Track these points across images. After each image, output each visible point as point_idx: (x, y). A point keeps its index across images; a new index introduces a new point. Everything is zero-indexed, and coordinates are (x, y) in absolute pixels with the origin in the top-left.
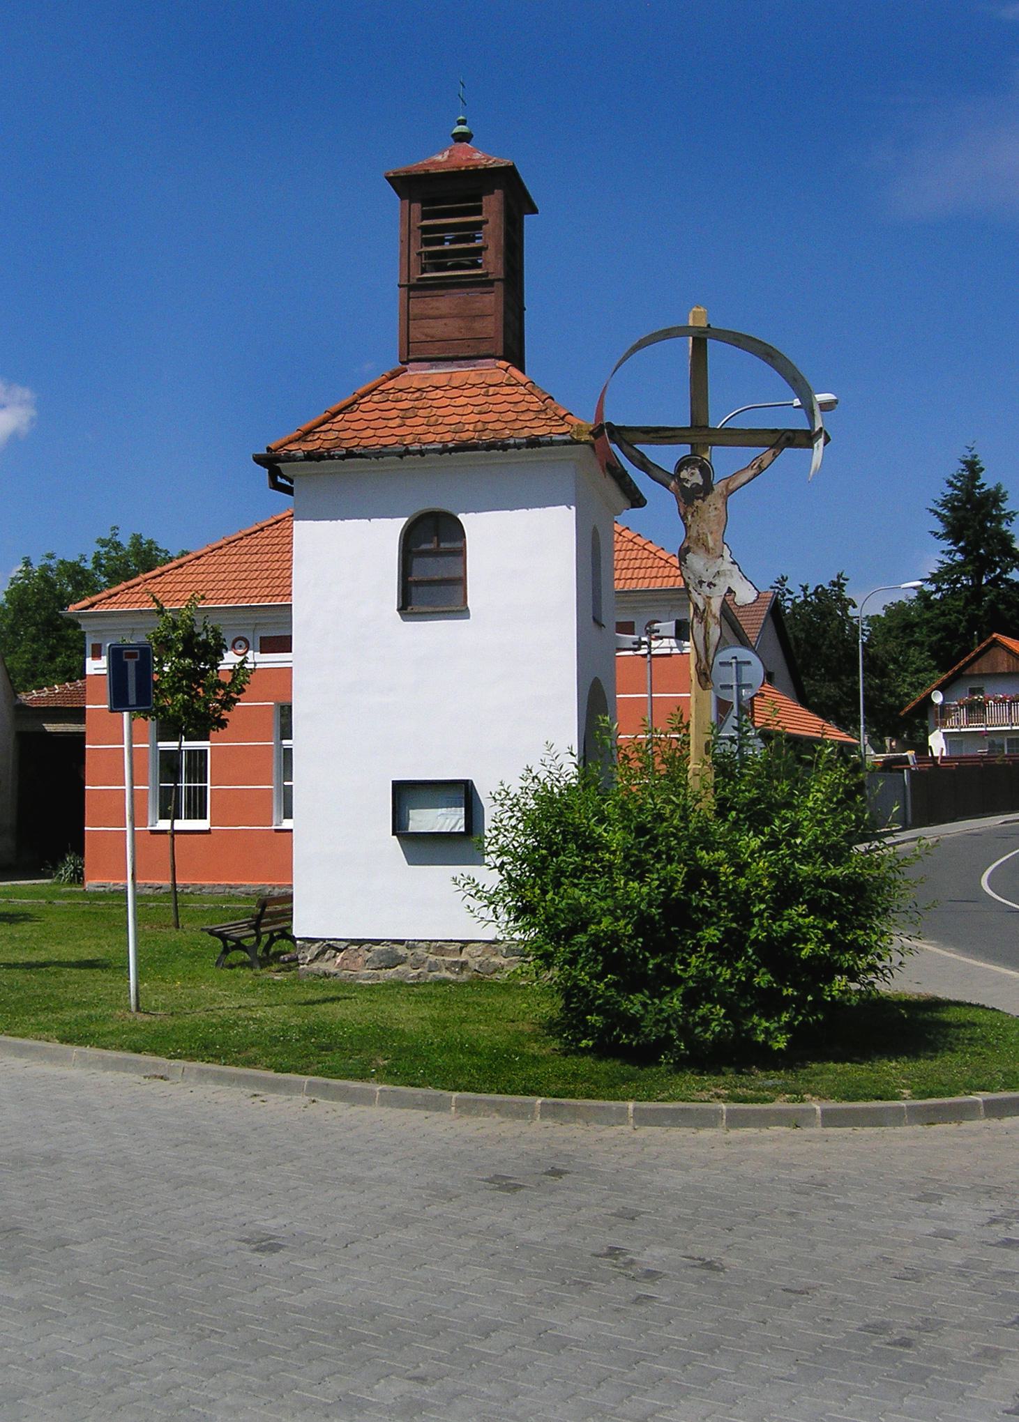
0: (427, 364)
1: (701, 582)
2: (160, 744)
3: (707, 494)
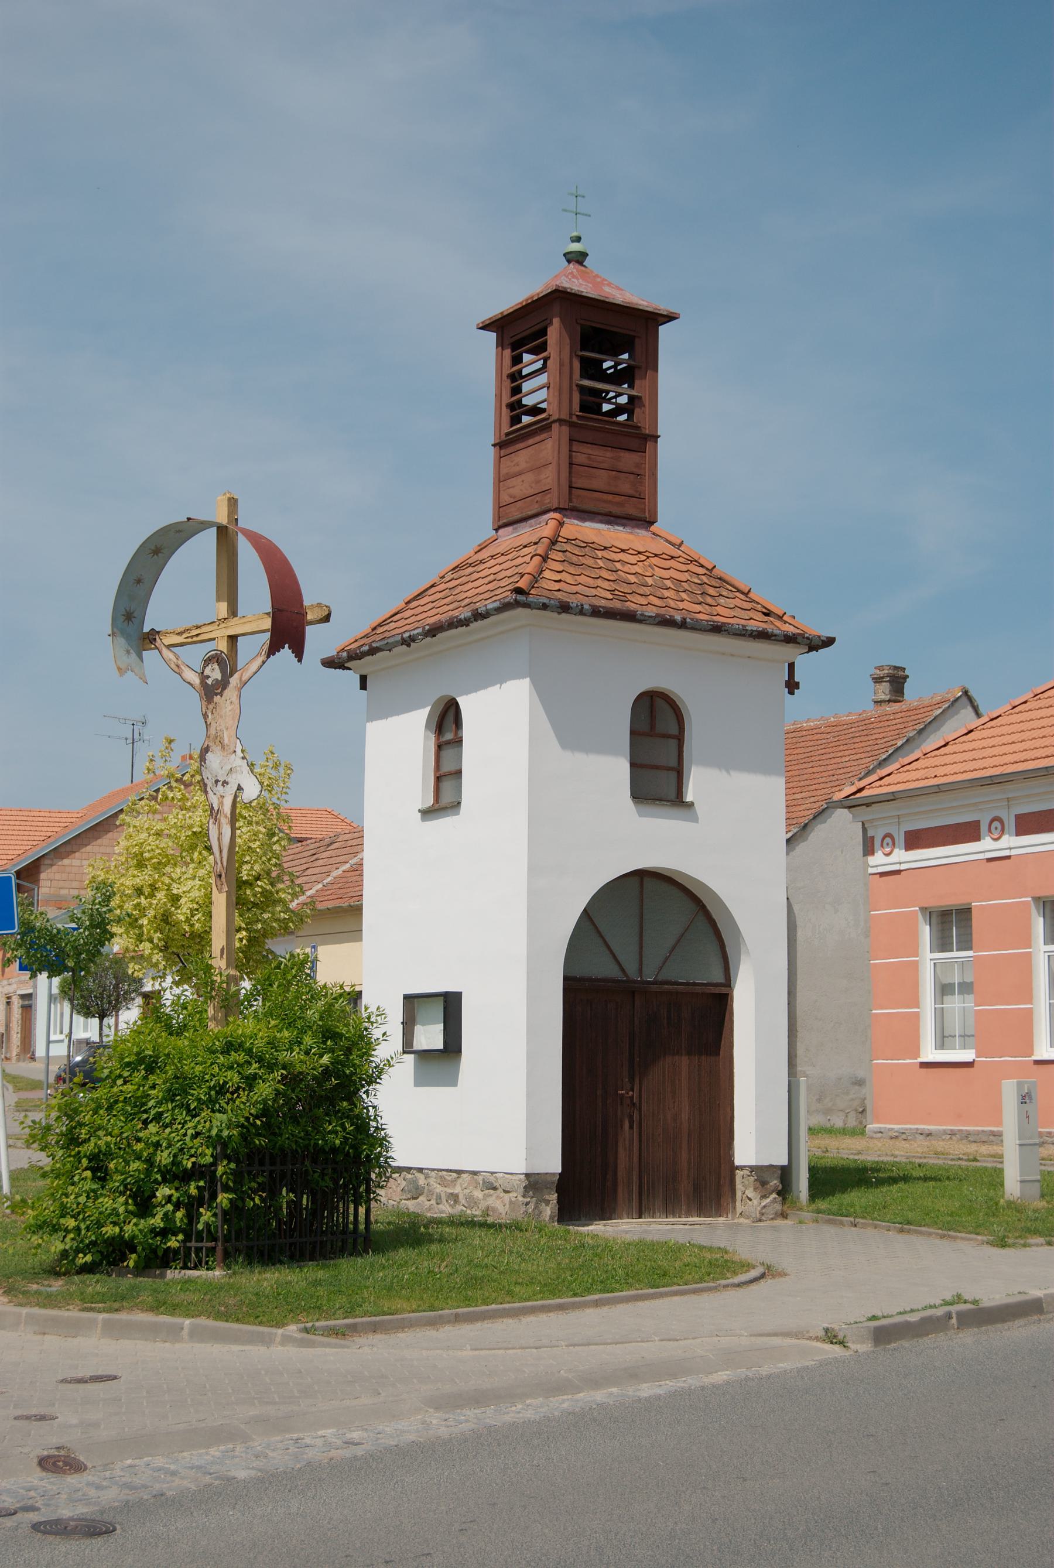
0: (510, 529)
3: (224, 688)
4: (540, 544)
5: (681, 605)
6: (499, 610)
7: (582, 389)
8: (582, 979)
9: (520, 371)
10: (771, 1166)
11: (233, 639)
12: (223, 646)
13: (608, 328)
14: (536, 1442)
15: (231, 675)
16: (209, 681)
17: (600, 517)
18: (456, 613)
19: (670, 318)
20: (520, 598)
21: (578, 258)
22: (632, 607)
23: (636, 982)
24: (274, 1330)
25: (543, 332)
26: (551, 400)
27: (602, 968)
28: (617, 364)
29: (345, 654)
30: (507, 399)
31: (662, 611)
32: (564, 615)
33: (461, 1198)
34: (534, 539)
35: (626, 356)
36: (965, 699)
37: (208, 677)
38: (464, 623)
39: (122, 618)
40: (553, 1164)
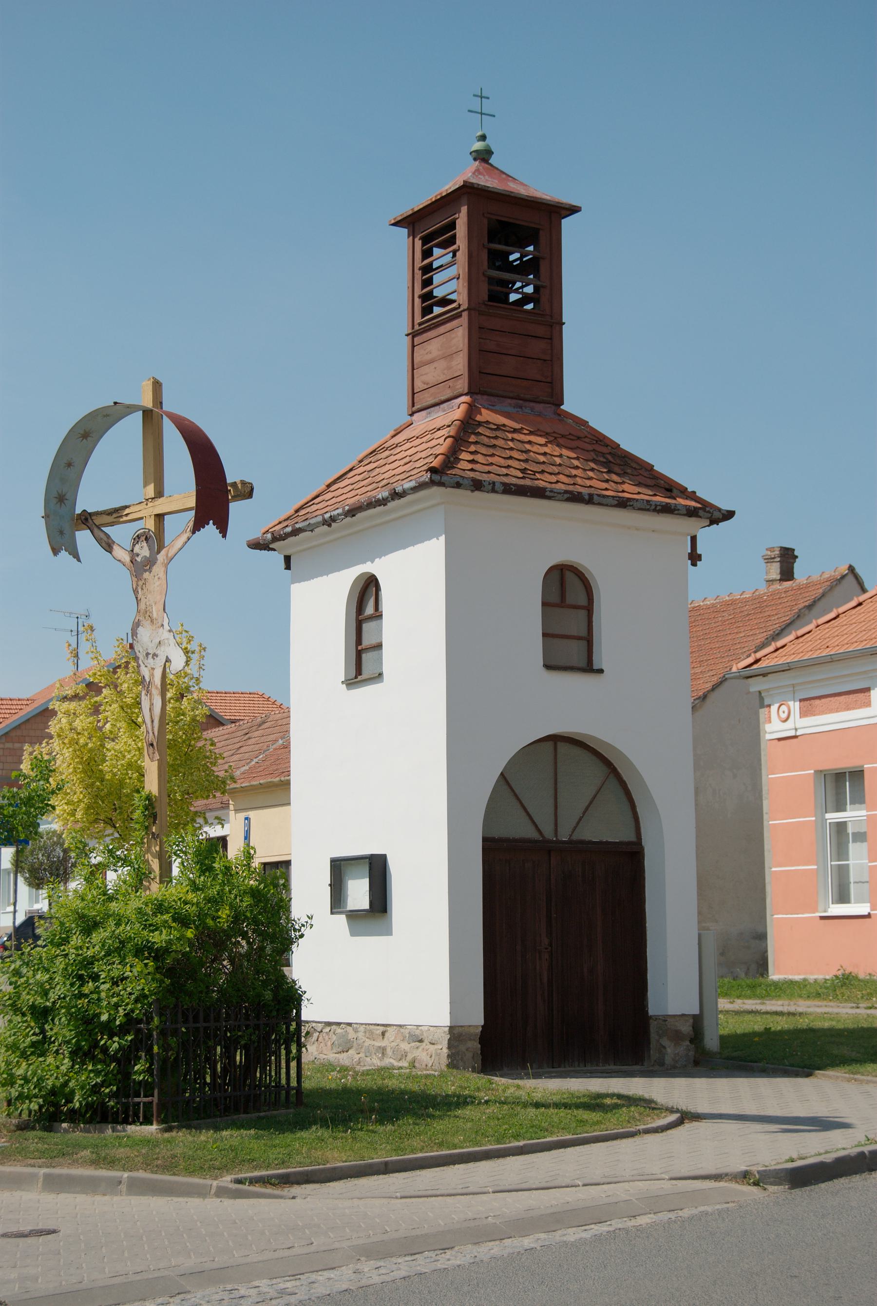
0: (424, 413)
1: (147, 654)
2: (828, 816)
4: (452, 427)
5: (588, 483)
6: (415, 489)
7: (491, 280)
8: (501, 840)
9: (431, 264)
10: (683, 1015)
11: (160, 518)
12: (150, 524)
13: (511, 221)
14: (466, 1288)
15: (159, 552)
16: (139, 559)
17: (509, 401)
18: (373, 493)
19: (573, 210)
20: (436, 478)
21: (484, 156)
22: (541, 484)
23: (552, 842)
24: (209, 1182)
25: (452, 226)
26: (461, 290)
27: (521, 830)
28: (522, 256)
29: (269, 536)
30: (418, 291)
31: (571, 488)
32: (477, 493)
33: (389, 1052)
34: (447, 422)
35: (531, 248)
36: (851, 578)
37: (138, 555)
38: (383, 502)
39: (55, 501)
40: (476, 1018)
